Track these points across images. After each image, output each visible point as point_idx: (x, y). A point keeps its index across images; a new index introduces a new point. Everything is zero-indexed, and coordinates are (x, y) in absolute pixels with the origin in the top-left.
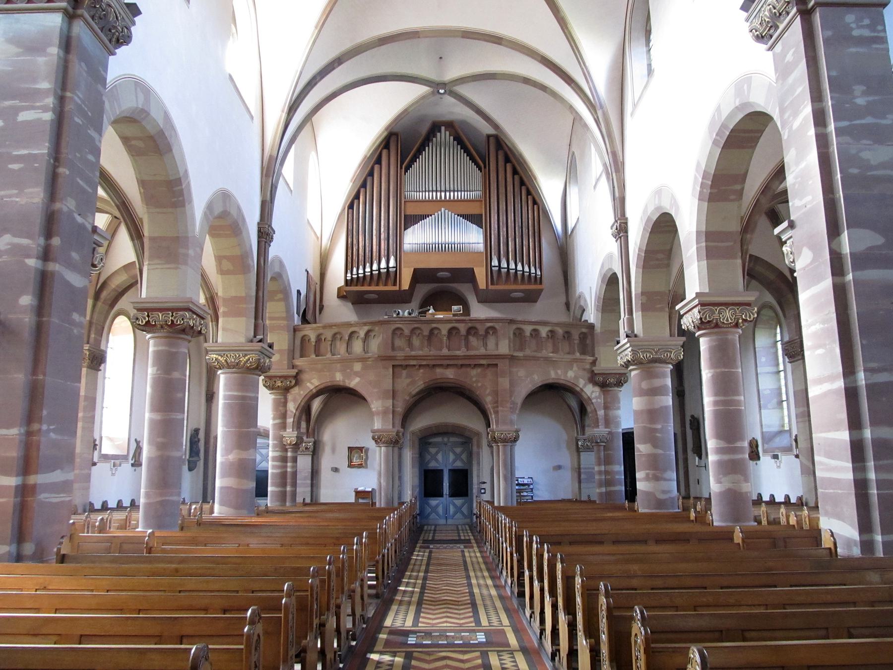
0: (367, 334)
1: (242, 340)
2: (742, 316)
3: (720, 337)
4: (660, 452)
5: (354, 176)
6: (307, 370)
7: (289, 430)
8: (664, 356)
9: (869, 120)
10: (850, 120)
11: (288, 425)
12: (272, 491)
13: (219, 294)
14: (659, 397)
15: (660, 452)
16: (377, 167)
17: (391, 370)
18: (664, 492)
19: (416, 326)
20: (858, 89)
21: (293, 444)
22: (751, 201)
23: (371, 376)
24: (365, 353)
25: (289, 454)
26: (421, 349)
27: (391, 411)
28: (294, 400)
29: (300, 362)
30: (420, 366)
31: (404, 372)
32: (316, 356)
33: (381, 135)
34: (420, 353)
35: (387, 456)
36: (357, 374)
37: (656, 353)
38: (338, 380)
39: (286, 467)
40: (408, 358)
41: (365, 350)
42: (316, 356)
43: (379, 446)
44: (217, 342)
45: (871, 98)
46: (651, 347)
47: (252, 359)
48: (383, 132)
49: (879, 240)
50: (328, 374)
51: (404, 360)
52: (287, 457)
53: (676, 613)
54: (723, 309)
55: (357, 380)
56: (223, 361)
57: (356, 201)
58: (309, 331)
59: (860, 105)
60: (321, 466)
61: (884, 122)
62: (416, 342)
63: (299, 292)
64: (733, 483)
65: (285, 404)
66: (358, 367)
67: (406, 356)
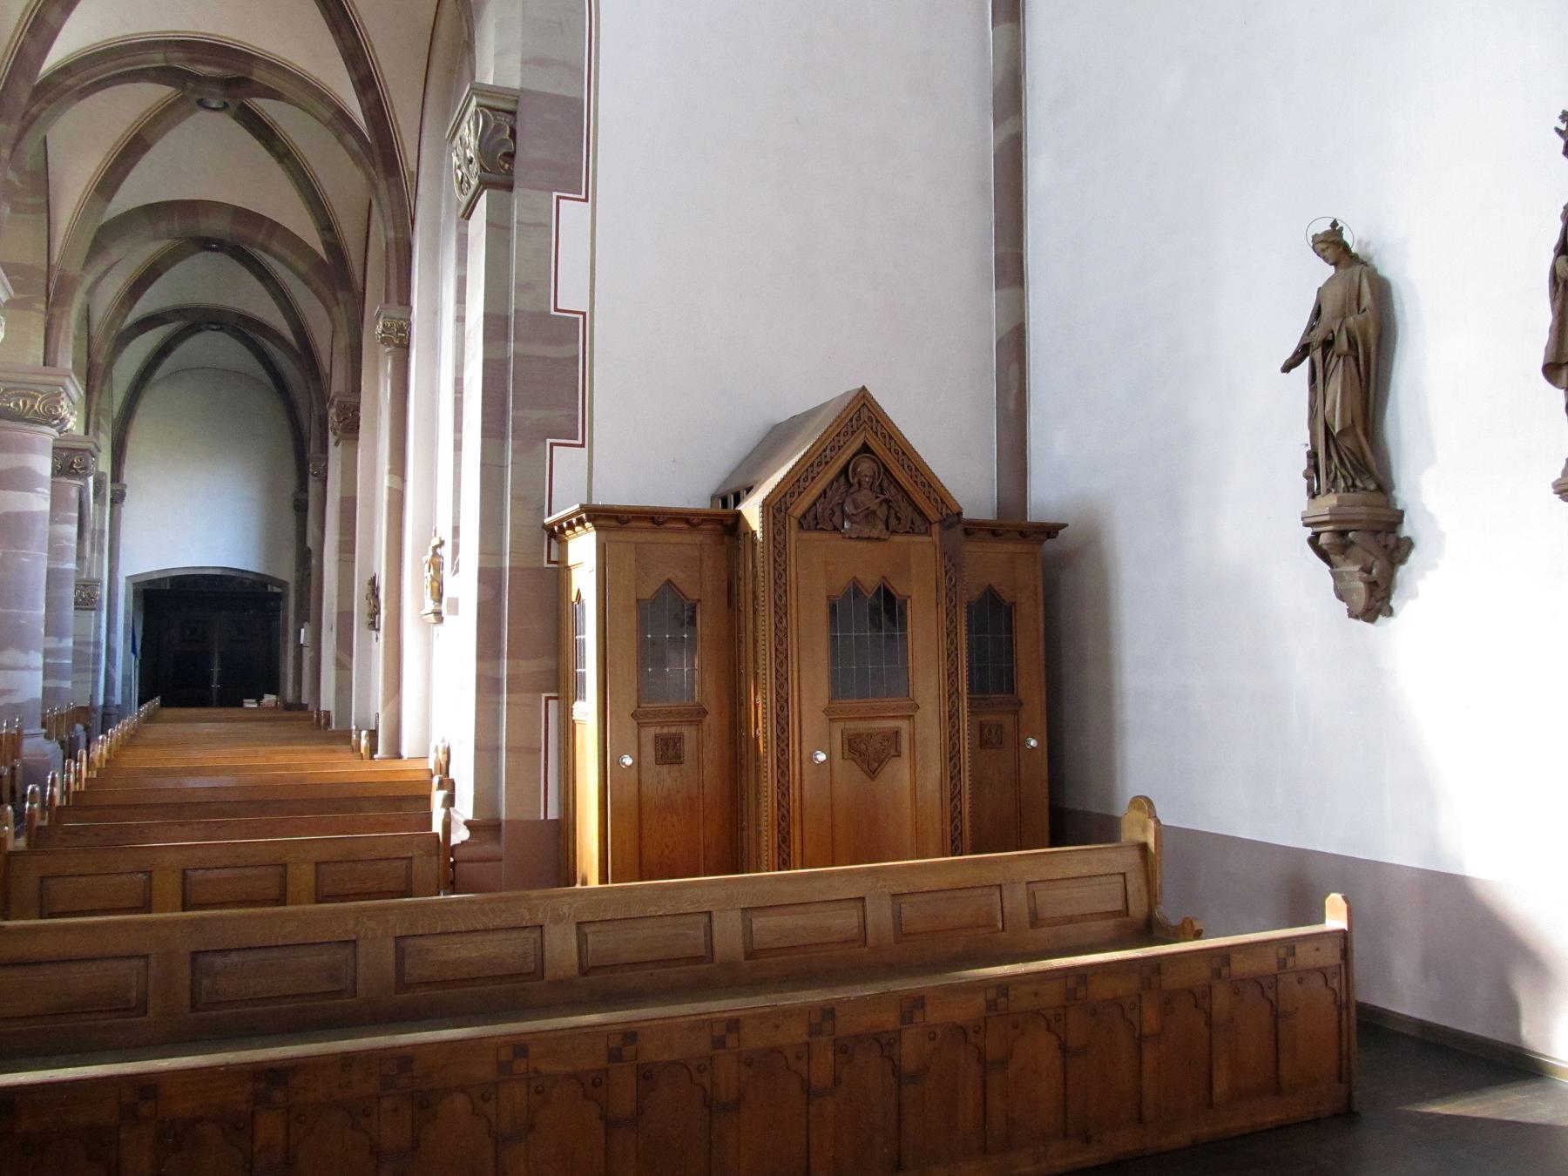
8: (17, 405)
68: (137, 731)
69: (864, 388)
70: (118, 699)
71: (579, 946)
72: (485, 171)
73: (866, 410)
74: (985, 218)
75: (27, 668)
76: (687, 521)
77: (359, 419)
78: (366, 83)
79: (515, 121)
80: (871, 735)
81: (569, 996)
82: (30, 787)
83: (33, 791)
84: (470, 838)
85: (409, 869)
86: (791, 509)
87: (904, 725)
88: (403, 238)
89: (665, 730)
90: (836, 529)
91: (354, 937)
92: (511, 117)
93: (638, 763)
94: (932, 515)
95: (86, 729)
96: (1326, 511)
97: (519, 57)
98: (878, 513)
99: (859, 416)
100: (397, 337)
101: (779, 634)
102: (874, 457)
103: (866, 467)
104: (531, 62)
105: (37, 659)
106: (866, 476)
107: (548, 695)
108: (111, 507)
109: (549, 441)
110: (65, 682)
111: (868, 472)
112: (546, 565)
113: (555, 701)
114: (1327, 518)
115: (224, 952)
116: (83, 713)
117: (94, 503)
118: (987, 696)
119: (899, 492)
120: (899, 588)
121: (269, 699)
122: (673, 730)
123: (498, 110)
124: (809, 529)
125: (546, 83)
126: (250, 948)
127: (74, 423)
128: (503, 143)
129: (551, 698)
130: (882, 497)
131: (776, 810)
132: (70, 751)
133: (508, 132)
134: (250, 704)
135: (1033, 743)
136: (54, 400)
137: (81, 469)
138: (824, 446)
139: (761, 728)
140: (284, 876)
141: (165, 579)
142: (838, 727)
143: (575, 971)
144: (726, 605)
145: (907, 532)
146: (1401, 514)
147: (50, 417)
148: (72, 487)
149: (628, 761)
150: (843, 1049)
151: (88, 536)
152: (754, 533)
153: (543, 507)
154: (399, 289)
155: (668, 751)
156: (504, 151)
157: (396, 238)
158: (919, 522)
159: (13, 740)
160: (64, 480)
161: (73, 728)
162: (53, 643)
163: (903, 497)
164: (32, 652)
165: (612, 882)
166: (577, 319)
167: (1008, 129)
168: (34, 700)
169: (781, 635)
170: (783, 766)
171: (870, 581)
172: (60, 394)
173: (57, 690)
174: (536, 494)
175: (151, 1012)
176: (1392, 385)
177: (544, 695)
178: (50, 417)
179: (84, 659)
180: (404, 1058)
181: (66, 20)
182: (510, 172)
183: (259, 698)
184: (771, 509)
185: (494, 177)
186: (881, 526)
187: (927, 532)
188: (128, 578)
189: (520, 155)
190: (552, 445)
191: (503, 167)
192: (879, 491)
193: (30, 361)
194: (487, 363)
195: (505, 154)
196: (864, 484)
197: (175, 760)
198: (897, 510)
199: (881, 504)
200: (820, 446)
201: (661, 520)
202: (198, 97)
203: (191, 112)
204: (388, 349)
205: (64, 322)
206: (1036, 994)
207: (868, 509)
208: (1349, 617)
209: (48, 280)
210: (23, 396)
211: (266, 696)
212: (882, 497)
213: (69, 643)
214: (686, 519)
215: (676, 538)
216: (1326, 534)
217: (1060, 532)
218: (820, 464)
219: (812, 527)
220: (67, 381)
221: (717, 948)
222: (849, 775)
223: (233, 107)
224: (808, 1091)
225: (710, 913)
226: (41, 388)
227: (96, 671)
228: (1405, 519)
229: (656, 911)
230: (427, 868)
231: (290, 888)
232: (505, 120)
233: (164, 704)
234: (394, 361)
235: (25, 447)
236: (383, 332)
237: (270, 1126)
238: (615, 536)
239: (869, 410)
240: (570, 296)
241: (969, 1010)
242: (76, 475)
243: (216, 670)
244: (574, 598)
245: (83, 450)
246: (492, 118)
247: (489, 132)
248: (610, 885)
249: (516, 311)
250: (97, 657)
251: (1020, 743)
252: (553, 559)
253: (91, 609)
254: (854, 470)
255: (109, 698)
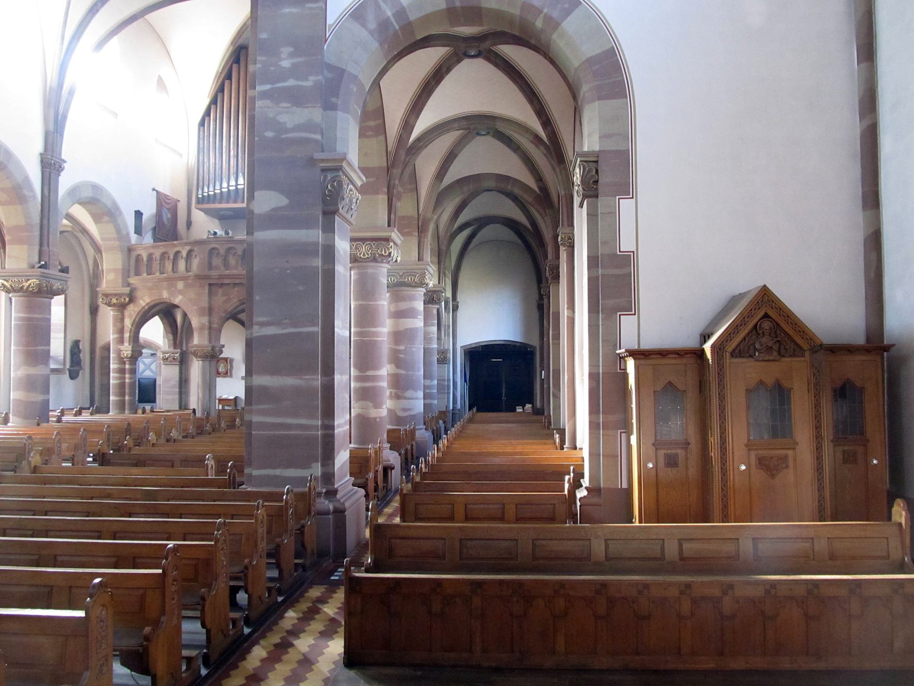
0: (190, 253)
1: (24, 265)
2: (377, 251)
3: (361, 271)
4: (403, 372)
5: (210, 91)
6: (141, 288)
7: (126, 344)
8: (408, 280)
9: (291, 83)
10: (272, 84)
11: (125, 339)
12: (113, 400)
13: (4, 224)
14: (404, 319)
15: (403, 372)
16: (227, 83)
17: (207, 288)
18: (404, 410)
19: (230, 245)
20: (286, 51)
21: (130, 357)
22: (396, 136)
23: (192, 294)
24: (187, 272)
25: (127, 366)
26: (236, 268)
27: (207, 327)
28: (130, 316)
29: (133, 280)
30: (235, 284)
31: (220, 291)
32: (148, 275)
33: (228, 50)
34: (235, 272)
35: (203, 369)
36: (180, 292)
37: (401, 276)
38: (165, 297)
39: (125, 378)
40: (221, 277)
41: (188, 269)
42: (148, 275)
43: (197, 360)
44: (5, 268)
45: (296, 60)
46: (396, 271)
47: (33, 284)
48: (230, 47)
49: (283, 201)
50: (156, 291)
51: (219, 278)
52: (125, 369)
53: (232, 521)
54: (360, 244)
55: (180, 297)
56: (9, 286)
57: (207, 118)
58: (142, 251)
59: (284, 67)
60: (190, 375)
61: (304, 84)
62: (232, 261)
63: (138, 214)
64: (362, 409)
65: (122, 320)
66: (180, 285)
67: (220, 275)
68: (463, 429)
69: (765, 286)
70: (459, 406)
71: (606, 551)
72: (585, 190)
73: (766, 297)
74: (854, 171)
75: (417, 399)
76: (678, 354)
77: (559, 272)
78: (547, 122)
79: (598, 166)
80: (772, 458)
81: (673, 569)
82: (412, 466)
83: (413, 467)
84: (588, 495)
85: (554, 509)
86: (726, 348)
87: (790, 452)
88: (569, 194)
89: (669, 452)
90: (751, 356)
91: (517, 538)
92: (596, 164)
93: (656, 466)
94: (805, 346)
95: (444, 422)
97: (598, 136)
98: (773, 347)
99: (763, 300)
100: (568, 242)
101: (721, 408)
102: (770, 320)
103: (766, 325)
104: (603, 137)
105: (421, 394)
106: (766, 329)
107: (621, 431)
108: (452, 313)
109: (618, 313)
110: (434, 401)
111: (767, 328)
112: (619, 371)
113: (625, 434)
115: (471, 539)
116: (443, 414)
117: (445, 312)
118: (847, 437)
119: (786, 336)
120: (786, 384)
121: (528, 406)
122: (673, 451)
123: (590, 162)
124: (736, 357)
125: (611, 145)
126: (657, 500)
127: (432, 282)
128: (592, 176)
129: (623, 432)
130: (776, 339)
131: (721, 492)
132: (436, 439)
133: (594, 171)
134: (519, 409)
135: (875, 462)
136: (423, 276)
137: (437, 300)
138: (744, 316)
139: (714, 454)
140: (503, 508)
141: (479, 347)
142: (753, 454)
143: (603, 559)
144: (699, 392)
145: (792, 356)
147: (422, 284)
148: (434, 309)
149: (650, 465)
150: (694, 601)
151: (443, 329)
152: (708, 359)
153: (617, 344)
154: (568, 217)
155: (672, 462)
156: (592, 181)
157: (565, 194)
158: (797, 351)
159: (412, 432)
160: (430, 306)
161: (438, 423)
162: (428, 382)
163: (788, 338)
164: (418, 391)
165: (644, 523)
166: (630, 255)
167: (867, 122)
168: (420, 413)
169: (722, 409)
170: (724, 471)
171: (770, 381)
172: (425, 273)
173: (431, 404)
174: (614, 340)
175: (447, 559)
177: (619, 431)
178: (422, 284)
179: (442, 388)
180: (520, 583)
182: (597, 189)
183: (524, 406)
184: (716, 349)
185: (590, 193)
186: (775, 354)
187: (803, 356)
188: (461, 347)
189: (600, 181)
190: (620, 315)
191: (593, 187)
192: (774, 336)
193: (413, 259)
194: (589, 279)
195: (594, 182)
196: (766, 334)
197: (473, 447)
198: (785, 344)
199: (775, 343)
200: (741, 316)
201: (665, 354)
202: (476, 131)
203: (473, 138)
204: (564, 248)
205: (426, 240)
206: (791, 590)
207: (767, 346)
209: (419, 221)
210: (410, 275)
211: (527, 405)
212: (776, 339)
213: (435, 382)
214: (679, 353)
215: (673, 361)
217: (891, 348)
218: (741, 325)
219: (738, 356)
220: (428, 267)
221: (666, 555)
222: (759, 476)
223: (492, 133)
224: (680, 616)
225: (663, 540)
226: (418, 271)
227: (448, 393)
229: (639, 537)
230: (561, 510)
231: (506, 514)
232: (593, 165)
233: (478, 411)
234: (567, 254)
235: (412, 298)
236: (561, 241)
237: (477, 601)
238: (642, 362)
239: (768, 296)
240: (626, 244)
241: (759, 592)
242: (436, 303)
243: (504, 391)
244: (630, 388)
245: (438, 291)
246: (587, 166)
247: (586, 172)
248: (643, 525)
249: (601, 255)
250: (449, 386)
251: (867, 462)
252: (622, 368)
253: (446, 364)
254: (760, 326)
255: (455, 406)
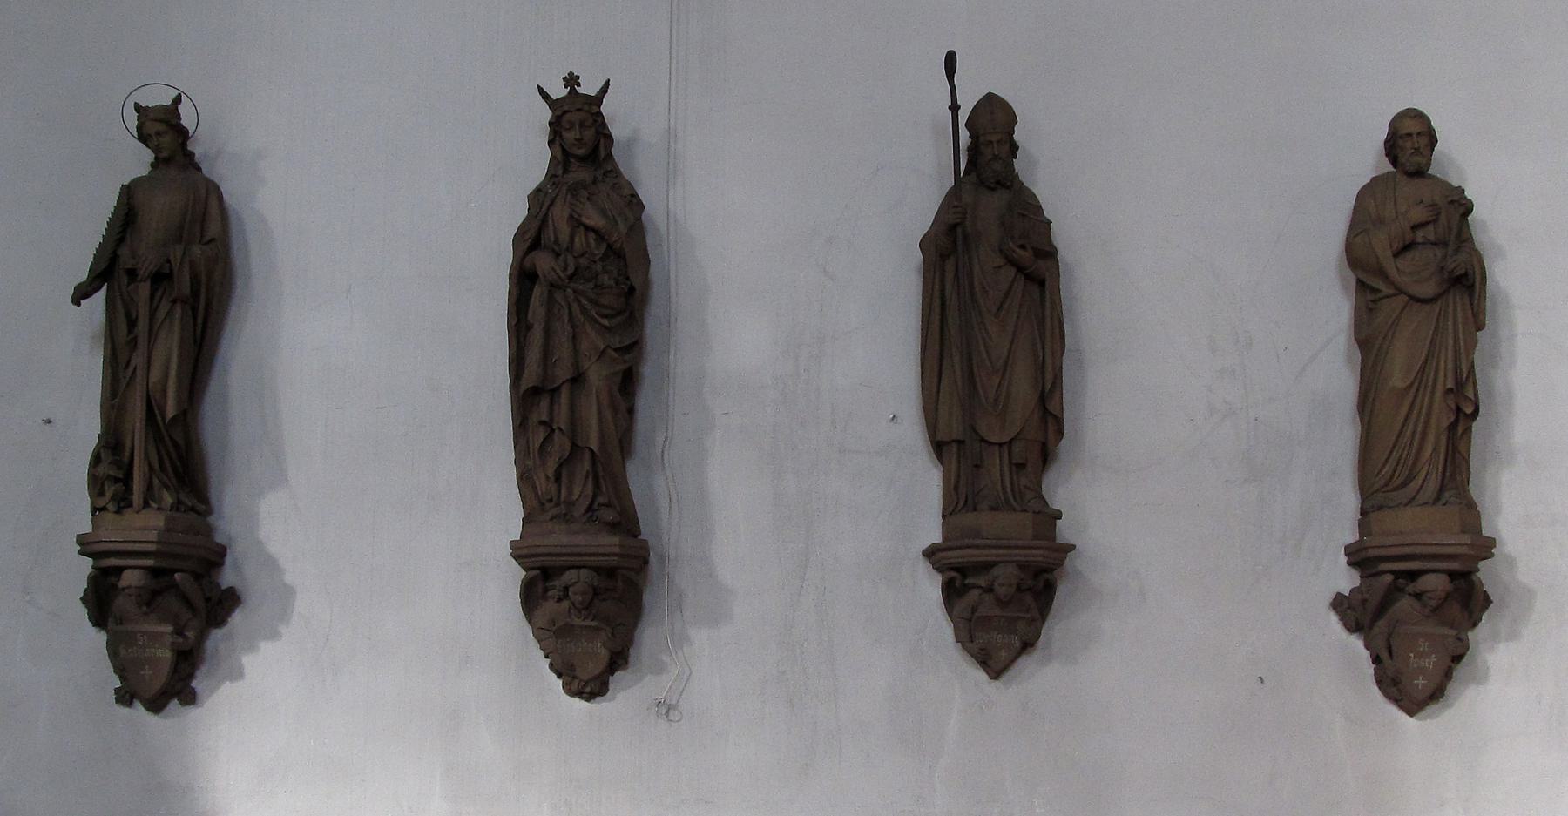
96: (153, 536)
114: (152, 547)
146: (221, 552)
176: (222, 352)
181: (1347, 255)
208: (117, 701)
216: (137, 572)
228: (228, 560)
